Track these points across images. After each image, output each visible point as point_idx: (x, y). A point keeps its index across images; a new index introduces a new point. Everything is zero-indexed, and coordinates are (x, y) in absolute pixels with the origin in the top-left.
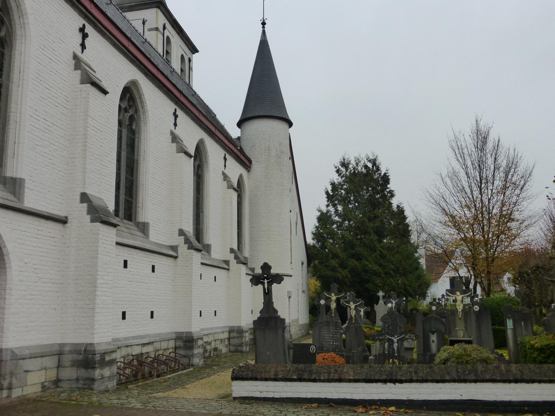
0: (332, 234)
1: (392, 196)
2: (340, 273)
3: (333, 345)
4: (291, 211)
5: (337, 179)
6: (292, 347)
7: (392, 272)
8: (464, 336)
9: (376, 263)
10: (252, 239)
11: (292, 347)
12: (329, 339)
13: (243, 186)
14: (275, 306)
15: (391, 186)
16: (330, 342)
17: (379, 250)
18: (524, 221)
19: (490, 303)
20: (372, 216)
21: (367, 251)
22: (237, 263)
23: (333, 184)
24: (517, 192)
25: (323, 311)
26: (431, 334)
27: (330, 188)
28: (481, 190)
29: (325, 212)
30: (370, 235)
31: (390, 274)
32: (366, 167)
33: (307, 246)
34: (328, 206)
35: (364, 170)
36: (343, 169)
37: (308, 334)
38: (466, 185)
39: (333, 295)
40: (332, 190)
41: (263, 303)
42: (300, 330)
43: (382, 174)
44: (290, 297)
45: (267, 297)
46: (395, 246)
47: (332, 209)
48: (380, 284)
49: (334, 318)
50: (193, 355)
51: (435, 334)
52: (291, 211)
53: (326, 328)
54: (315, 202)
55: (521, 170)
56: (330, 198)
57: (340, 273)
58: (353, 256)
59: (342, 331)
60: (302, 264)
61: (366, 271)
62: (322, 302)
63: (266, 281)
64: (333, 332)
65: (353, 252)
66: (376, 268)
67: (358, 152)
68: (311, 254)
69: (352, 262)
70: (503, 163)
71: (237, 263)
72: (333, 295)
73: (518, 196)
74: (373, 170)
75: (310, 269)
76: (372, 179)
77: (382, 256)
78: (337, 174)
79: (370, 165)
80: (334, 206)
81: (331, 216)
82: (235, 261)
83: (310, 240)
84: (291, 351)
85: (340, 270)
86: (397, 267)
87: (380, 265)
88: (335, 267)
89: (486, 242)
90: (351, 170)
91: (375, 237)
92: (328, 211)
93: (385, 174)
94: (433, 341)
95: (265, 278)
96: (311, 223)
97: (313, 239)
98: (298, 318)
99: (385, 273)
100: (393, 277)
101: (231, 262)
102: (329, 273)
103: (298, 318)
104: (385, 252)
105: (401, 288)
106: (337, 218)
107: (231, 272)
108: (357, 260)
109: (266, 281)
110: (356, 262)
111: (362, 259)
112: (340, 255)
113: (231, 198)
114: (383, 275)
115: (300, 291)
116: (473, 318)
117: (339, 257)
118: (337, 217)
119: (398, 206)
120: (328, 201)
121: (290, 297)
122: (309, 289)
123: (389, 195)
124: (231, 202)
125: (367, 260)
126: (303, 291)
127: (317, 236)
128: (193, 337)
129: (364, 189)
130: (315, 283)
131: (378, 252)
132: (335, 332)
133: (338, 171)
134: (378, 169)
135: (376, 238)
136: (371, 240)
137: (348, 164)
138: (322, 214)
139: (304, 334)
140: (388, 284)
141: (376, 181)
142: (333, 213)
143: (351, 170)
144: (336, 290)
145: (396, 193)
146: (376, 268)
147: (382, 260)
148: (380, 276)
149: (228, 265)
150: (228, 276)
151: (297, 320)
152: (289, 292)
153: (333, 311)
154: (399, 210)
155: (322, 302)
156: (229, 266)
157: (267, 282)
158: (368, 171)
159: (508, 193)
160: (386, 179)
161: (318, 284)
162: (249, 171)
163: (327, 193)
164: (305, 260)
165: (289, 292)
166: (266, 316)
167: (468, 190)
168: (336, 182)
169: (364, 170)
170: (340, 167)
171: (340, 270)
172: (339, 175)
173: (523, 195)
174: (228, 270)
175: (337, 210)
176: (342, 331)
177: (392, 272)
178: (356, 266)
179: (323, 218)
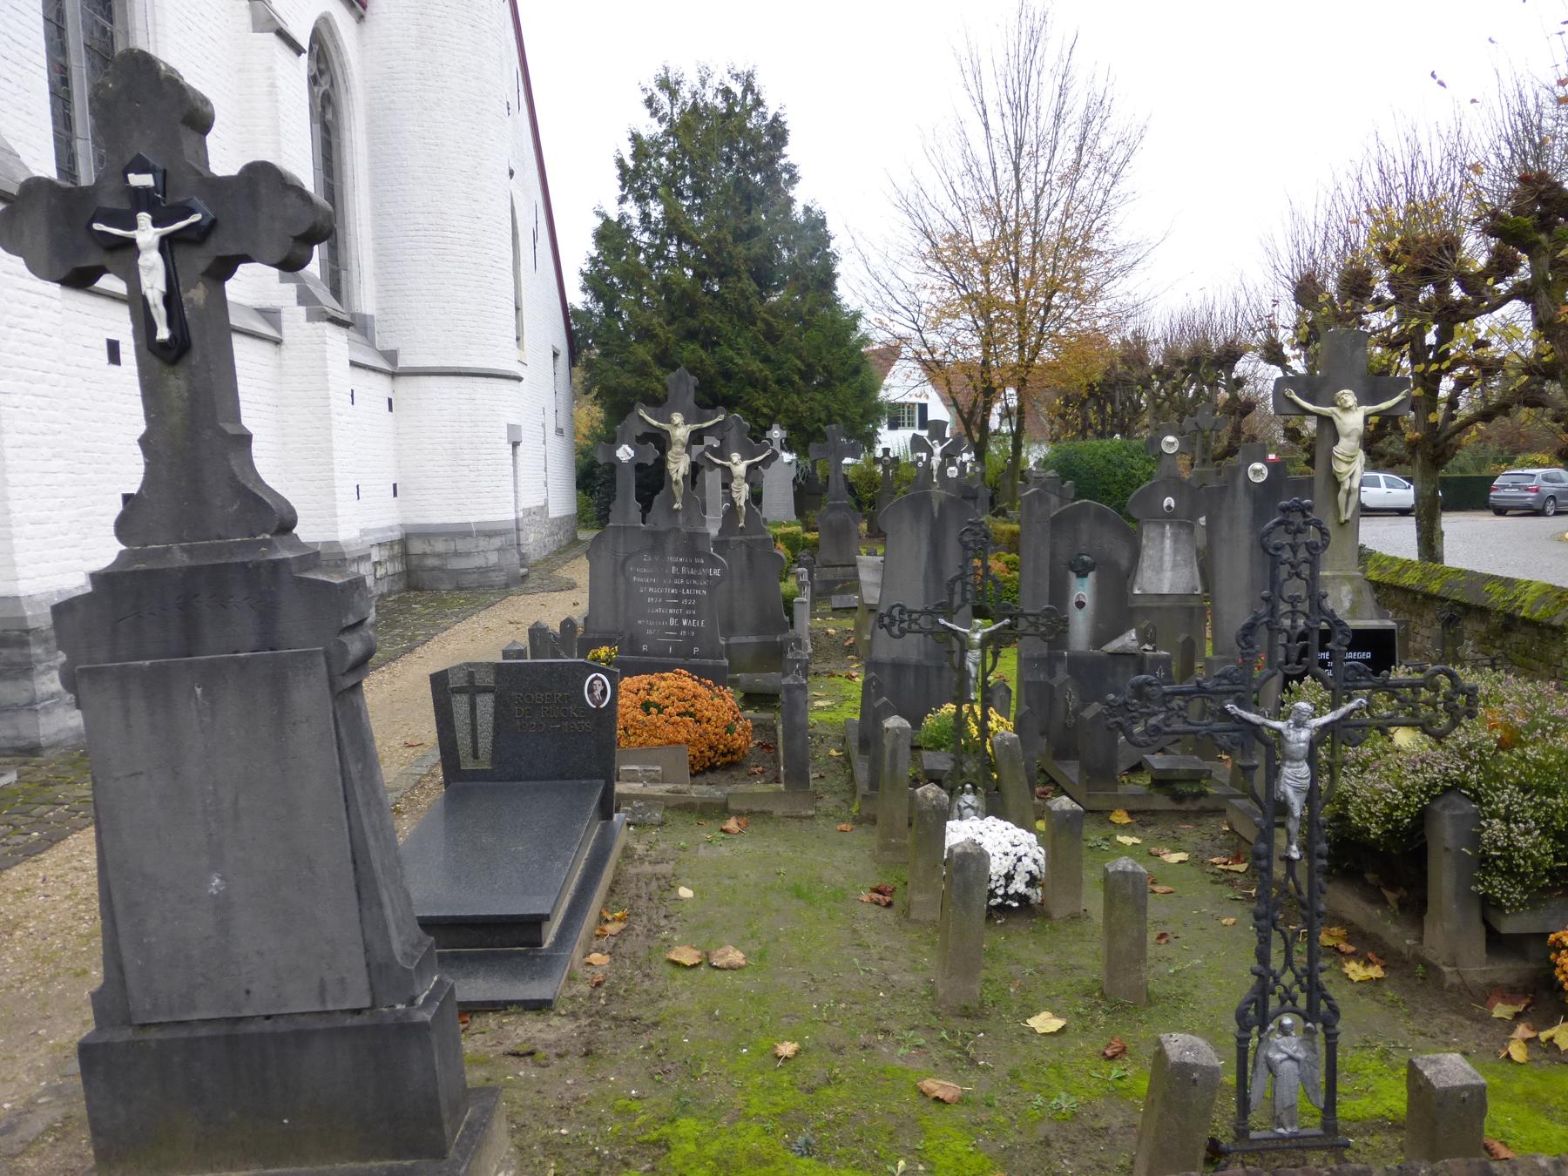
0: (633, 277)
1: (794, 179)
2: (658, 380)
3: (679, 628)
4: (511, 173)
5: (651, 128)
6: (489, 681)
7: (796, 378)
8: (1354, 612)
9: (755, 353)
10: (384, 256)
11: (489, 681)
12: (665, 605)
13: (342, 66)
14: (272, 464)
15: (792, 153)
16: (666, 617)
17: (764, 320)
18: (1116, 253)
19: (1086, 457)
20: (745, 227)
21: (730, 321)
22: (309, 319)
23: (636, 138)
24: (1107, 179)
25: (627, 486)
26: (1072, 575)
27: (627, 151)
28: (1017, 169)
29: (616, 219)
30: (740, 279)
31: (792, 383)
32: (727, 93)
33: (568, 313)
34: (623, 200)
35: (719, 103)
36: (663, 98)
37: (575, 542)
38: (984, 158)
39: (677, 418)
40: (634, 156)
41: (144, 442)
42: (552, 534)
43: (770, 117)
44: (515, 445)
45: (176, 384)
46: (805, 310)
47: (632, 210)
48: (765, 410)
49: (681, 519)
50: (32, 703)
51: (1091, 575)
52: (511, 173)
53: (646, 558)
54: (589, 194)
55: (1116, 124)
56: (631, 178)
57: (658, 380)
58: (691, 335)
59: (717, 572)
60: (555, 355)
61: (727, 375)
62: (625, 453)
63: (147, 234)
64: (676, 576)
65: (693, 323)
66: (755, 365)
67: (706, 63)
68: (579, 335)
69: (692, 351)
70: (1076, 108)
71: (309, 319)
72: (677, 418)
73: (1107, 192)
74: (743, 106)
75: (576, 370)
76: (742, 129)
77: (772, 336)
78: (648, 111)
79: (737, 89)
80: (641, 199)
81: (629, 230)
82: (302, 309)
83: (578, 298)
84: (486, 703)
85: (658, 372)
86: (809, 366)
87: (766, 360)
88: (644, 363)
89: (1020, 308)
90: (685, 103)
91: (750, 286)
92: (622, 218)
93: (776, 118)
94: (1080, 605)
95: (142, 199)
96: (579, 250)
97: (584, 290)
98: (546, 501)
99: (779, 382)
100: (799, 393)
101: (284, 316)
102: (629, 381)
103: (546, 501)
104: (779, 325)
105: (820, 420)
106: (645, 237)
107: (288, 351)
108: (704, 346)
109: (147, 234)
110: (702, 352)
111: (717, 344)
112: (658, 331)
113: (270, 69)
114: (775, 387)
115: (551, 430)
116: (1243, 508)
117: (656, 336)
118: (647, 234)
119: (807, 210)
120: (622, 188)
121: (515, 445)
122: (575, 433)
123: (785, 176)
124: (273, 85)
125: (731, 347)
126: (559, 431)
127: (595, 283)
128: (23, 619)
129: (716, 165)
130: (592, 414)
131: (759, 323)
132: (690, 577)
133: (649, 102)
134: (758, 103)
135: (754, 286)
136: (742, 292)
137: (678, 83)
138: (607, 221)
139: (564, 543)
140: (787, 410)
141: (754, 137)
142: (636, 222)
143: (685, 103)
144: (690, 400)
145: (800, 171)
146: (755, 365)
147: (769, 346)
148: (765, 390)
149: (277, 325)
150: (280, 366)
151: (543, 509)
152: (513, 429)
153: (678, 490)
154: (808, 218)
155: (625, 453)
156: (279, 331)
157: (167, 246)
158: (730, 108)
159: (1082, 184)
160: (778, 133)
161: (598, 413)
162: (361, 18)
163: (621, 163)
164: (562, 345)
165: (513, 429)
166: (180, 558)
167: (988, 173)
168: (645, 135)
169: (719, 103)
170: (656, 90)
171: (658, 372)
172: (654, 114)
173: (1122, 187)
174: (277, 342)
175: (645, 217)
176: (717, 572)
177: (796, 378)
178: (702, 361)
179: (610, 235)
